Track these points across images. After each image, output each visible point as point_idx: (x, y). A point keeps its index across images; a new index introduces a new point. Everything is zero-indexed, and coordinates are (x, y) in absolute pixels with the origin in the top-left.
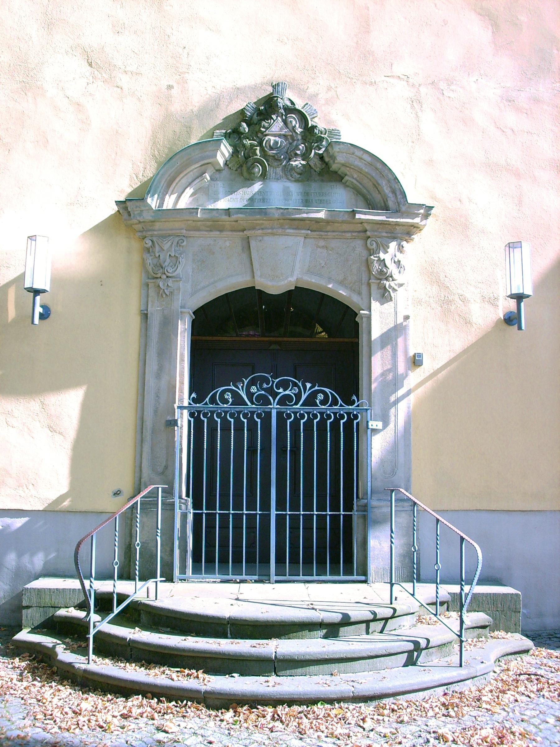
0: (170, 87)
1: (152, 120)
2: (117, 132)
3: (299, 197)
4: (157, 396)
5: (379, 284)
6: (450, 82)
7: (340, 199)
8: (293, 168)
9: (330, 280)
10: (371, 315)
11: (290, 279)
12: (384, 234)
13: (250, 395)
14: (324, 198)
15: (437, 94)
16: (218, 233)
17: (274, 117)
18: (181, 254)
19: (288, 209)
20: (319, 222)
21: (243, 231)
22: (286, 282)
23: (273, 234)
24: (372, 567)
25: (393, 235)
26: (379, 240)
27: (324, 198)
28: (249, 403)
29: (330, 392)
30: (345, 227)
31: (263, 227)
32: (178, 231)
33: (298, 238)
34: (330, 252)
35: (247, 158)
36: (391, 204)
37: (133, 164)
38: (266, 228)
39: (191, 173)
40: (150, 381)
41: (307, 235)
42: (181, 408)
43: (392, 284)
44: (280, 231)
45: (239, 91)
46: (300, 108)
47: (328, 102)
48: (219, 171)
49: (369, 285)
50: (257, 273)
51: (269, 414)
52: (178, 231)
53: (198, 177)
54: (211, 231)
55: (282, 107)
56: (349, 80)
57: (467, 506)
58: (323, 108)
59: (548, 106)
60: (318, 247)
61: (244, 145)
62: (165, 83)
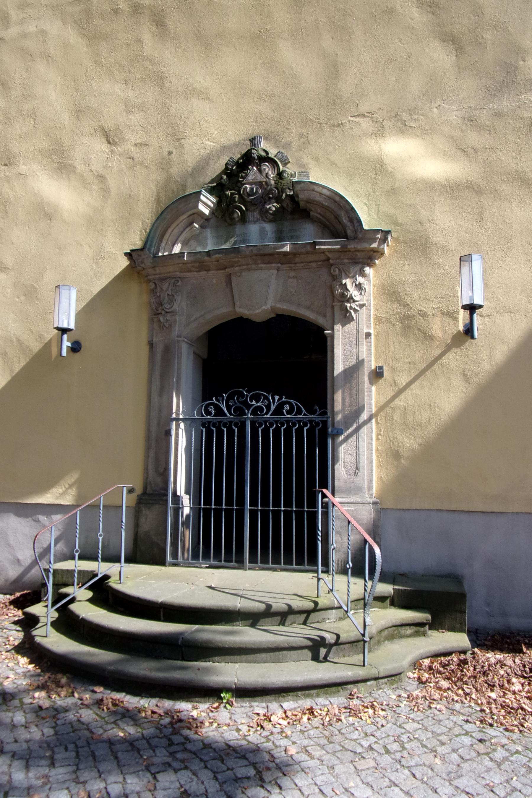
0: (170, 153)
1: (157, 183)
2: (130, 196)
3: (273, 235)
4: (160, 411)
5: (340, 307)
6: (412, 111)
7: (308, 233)
8: (267, 211)
9: (299, 305)
10: (334, 334)
11: (264, 307)
12: (346, 261)
13: (229, 408)
14: (294, 234)
15: (400, 125)
16: (205, 272)
17: (250, 167)
18: (176, 293)
19: (257, 246)
20: (286, 255)
21: (225, 269)
22: (260, 310)
23: (249, 270)
24: (335, 558)
25: (354, 261)
26: (341, 267)
27: (294, 234)
28: (228, 415)
29: (297, 405)
30: (311, 258)
31: (239, 264)
32: (173, 274)
33: (271, 271)
34: (300, 281)
35: (228, 206)
36: (350, 233)
37: (143, 221)
38: (243, 265)
39: (182, 223)
40: (155, 398)
41: (278, 267)
42: (177, 420)
43: (354, 305)
44: (254, 266)
45: (225, 148)
46: (273, 156)
47: (300, 148)
48: (207, 219)
49: (333, 307)
50: (238, 304)
51: (244, 423)
52: (173, 274)
53: (187, 227)
54: (200, 271)
55: (256, 157)
56: (319, 125)
57: (427, 507)
58: (296, 154)
59: (512, 119)
60: (289, 277)
61: (226, 195)
62: (166, 150)
